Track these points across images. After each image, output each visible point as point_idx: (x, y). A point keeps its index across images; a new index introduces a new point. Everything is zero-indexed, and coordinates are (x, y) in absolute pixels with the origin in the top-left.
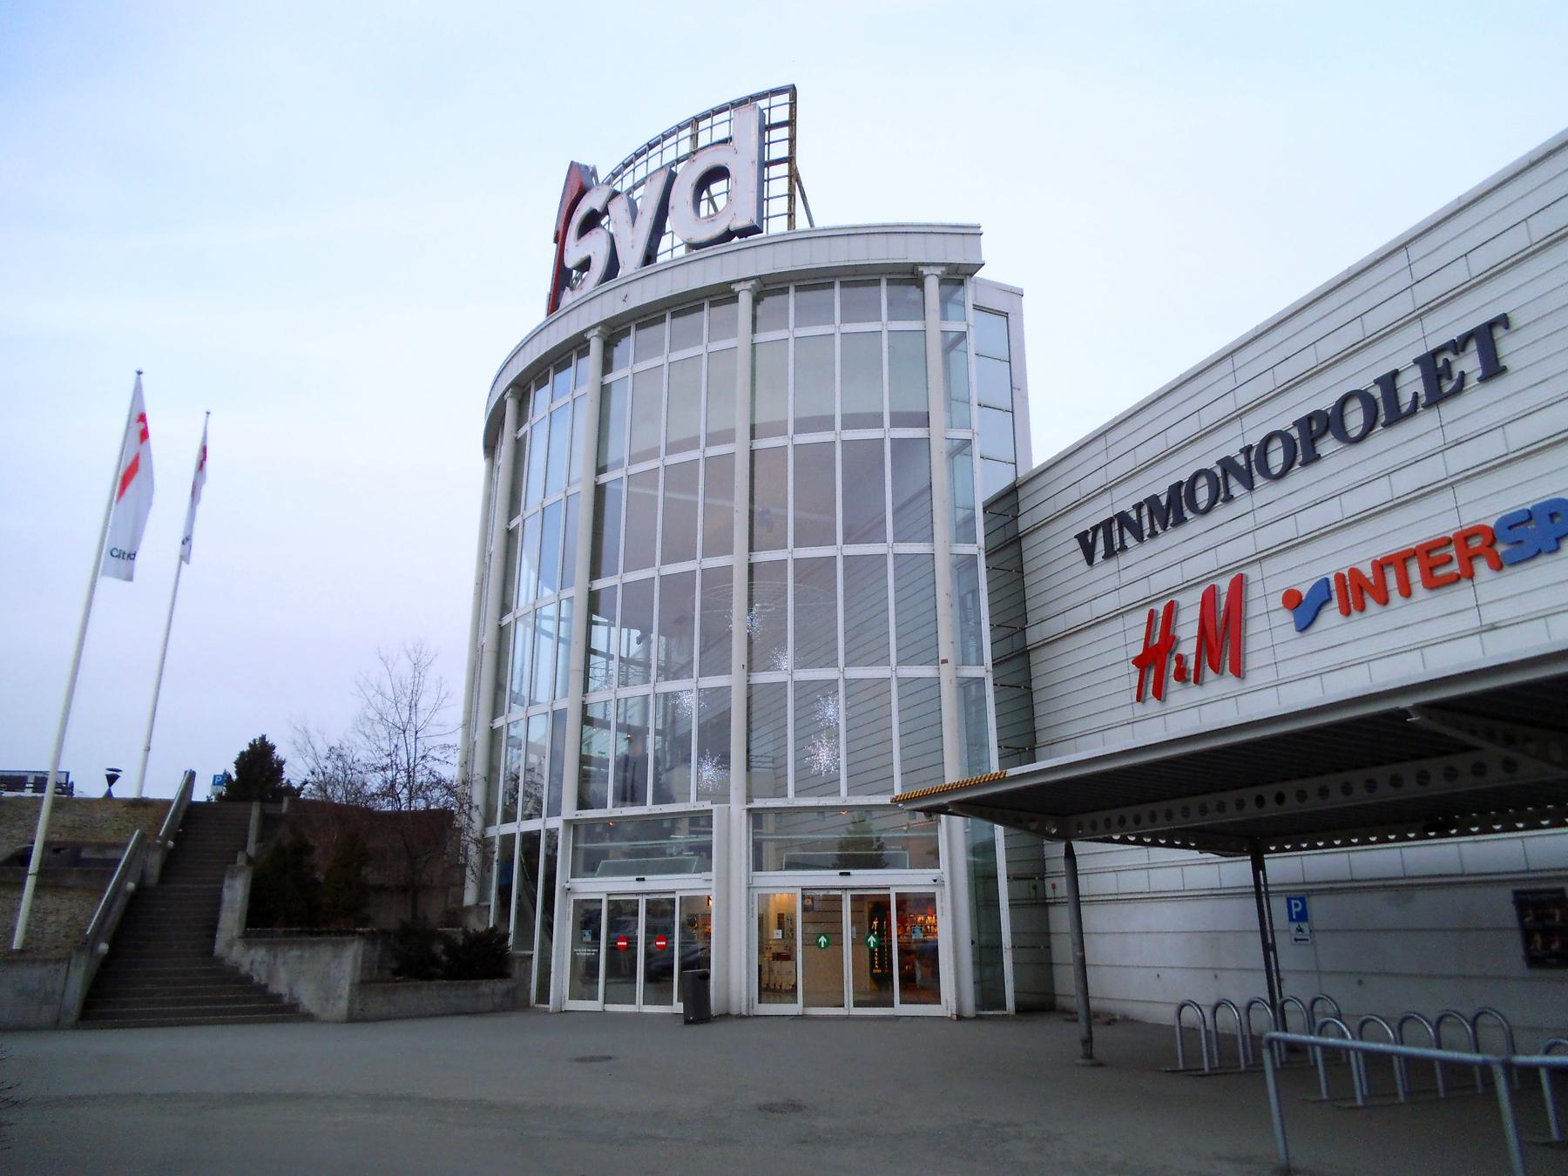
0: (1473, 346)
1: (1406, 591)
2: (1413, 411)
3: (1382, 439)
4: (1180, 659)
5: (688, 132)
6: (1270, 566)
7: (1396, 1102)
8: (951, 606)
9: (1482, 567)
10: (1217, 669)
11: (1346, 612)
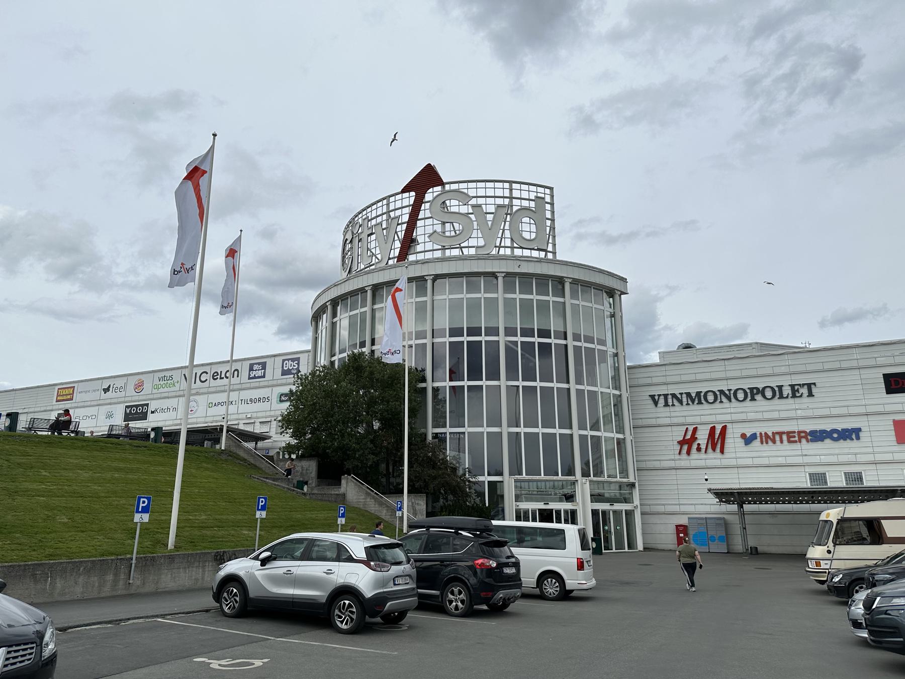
0: (806, 387)
1: (782, 442)
2: (787, 397)
3: (776, 401)
4: (699, 444)
5: (385, 202)
6: (735, 425)
7: (390, 476)
8: (688, 347)
9: (804, 440)
10: (714, 449)
11: (762, 443)
